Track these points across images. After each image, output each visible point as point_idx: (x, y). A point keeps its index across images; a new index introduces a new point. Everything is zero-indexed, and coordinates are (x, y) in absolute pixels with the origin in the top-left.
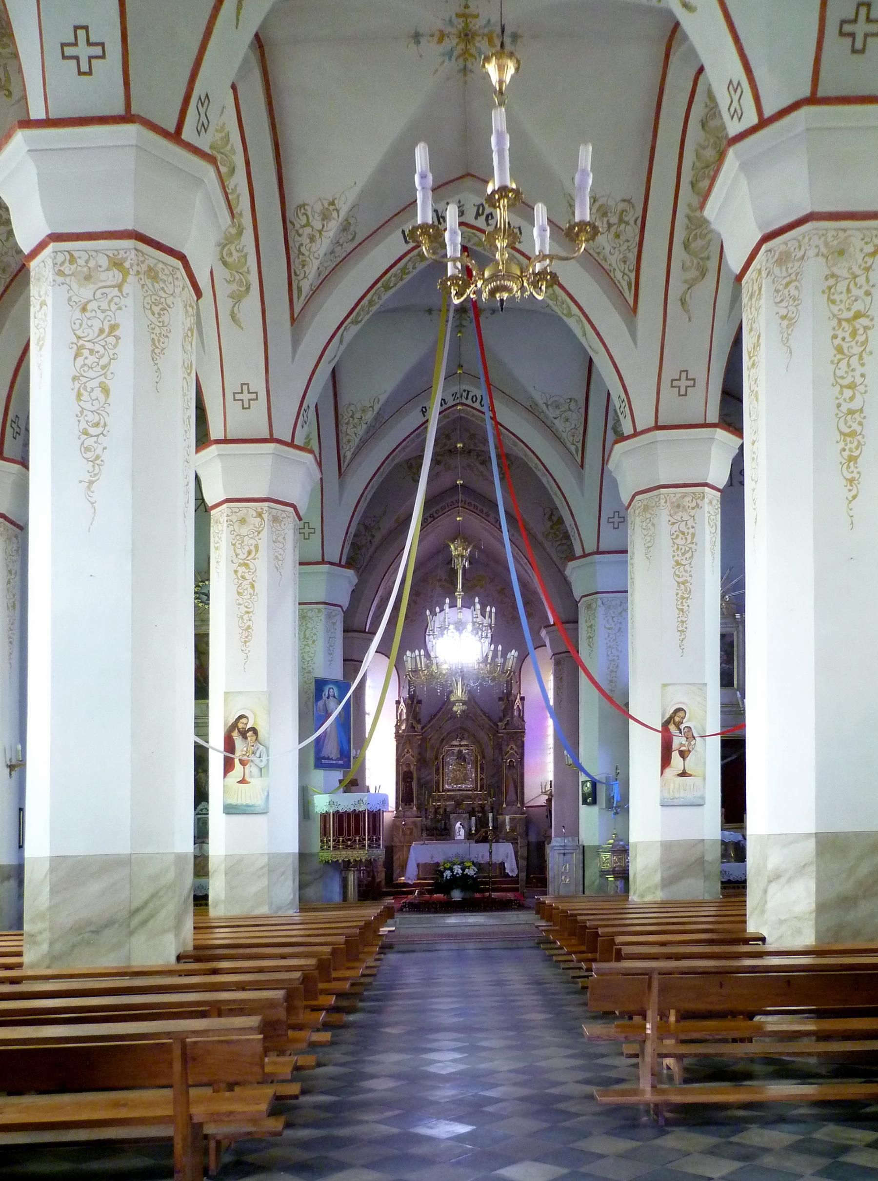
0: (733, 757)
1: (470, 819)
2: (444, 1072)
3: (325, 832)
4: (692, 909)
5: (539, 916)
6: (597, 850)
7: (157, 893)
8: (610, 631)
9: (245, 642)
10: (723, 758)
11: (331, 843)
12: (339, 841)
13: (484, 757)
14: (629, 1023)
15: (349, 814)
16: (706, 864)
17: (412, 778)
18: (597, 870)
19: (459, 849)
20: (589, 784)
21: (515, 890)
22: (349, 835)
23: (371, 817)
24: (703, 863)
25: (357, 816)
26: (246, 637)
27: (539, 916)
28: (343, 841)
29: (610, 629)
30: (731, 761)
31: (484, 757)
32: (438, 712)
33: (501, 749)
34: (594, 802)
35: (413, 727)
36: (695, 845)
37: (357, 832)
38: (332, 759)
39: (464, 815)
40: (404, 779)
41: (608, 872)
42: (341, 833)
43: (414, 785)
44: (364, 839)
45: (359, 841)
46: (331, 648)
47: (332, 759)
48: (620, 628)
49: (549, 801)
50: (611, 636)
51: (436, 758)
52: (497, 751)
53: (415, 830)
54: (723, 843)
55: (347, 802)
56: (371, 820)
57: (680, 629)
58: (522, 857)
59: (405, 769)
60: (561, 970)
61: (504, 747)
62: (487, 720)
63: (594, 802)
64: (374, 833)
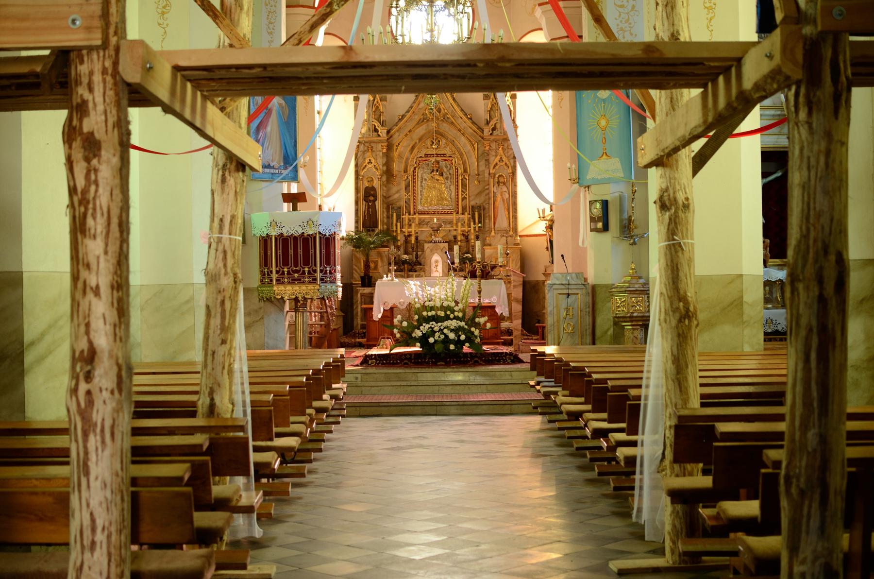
0: (779, 174)
1: (451, 249)
2: (417, 558)
3: (265, 260)
4: (726, 362)
5: (535, 373)
6: (610, 290)
7: (56, 322)
8: (621, 10)
9: (163, 13)
10: (764, 175)
11: (274, 276)
12: (283, 273)
13: (465, 171)
14: (425, 31)
15: (295, 238)
16: (745, 306)
17: (375, 196)
18: (611, 316)
19: (434, 287)
20: (598, 206)
21: (509, 343)
22: (296, 266)
23: (323, 242)
24: (742, 304)
25: (306, 241)
26: (164, 7)
27: (535, 373)
28: (289, 273)
29: (622, 6)
30: (777, 178)
31: (465, 171)
32: (408, 111)
33: (487, 161)
34: (606, 228)
35: (376, 130)
36: (732, 282)
37: (306, 262)
38: (273, 168)
39: (442, 245)
40: (366, 199)
41: (624, 319)
42: (286, 263)
43: (378, 204)
44: (315, 271)
45: (309, 273)
46: (271, 26)
47: (273, 168)
48: (633, 7)
49: (550, 227)
50: (623, 15)
51: (405, 171)
52: (482, 163)
53: (380, 263)
54: (767, 283)
55: (291, 222)
56: (323, 246)
57: (708, 5)
58: (517, 300)
59: (367, 184)
60: (566, 440)
61: (492, 159)
62: (469, 122)
63: (606, 228)
64: (328, 263)
